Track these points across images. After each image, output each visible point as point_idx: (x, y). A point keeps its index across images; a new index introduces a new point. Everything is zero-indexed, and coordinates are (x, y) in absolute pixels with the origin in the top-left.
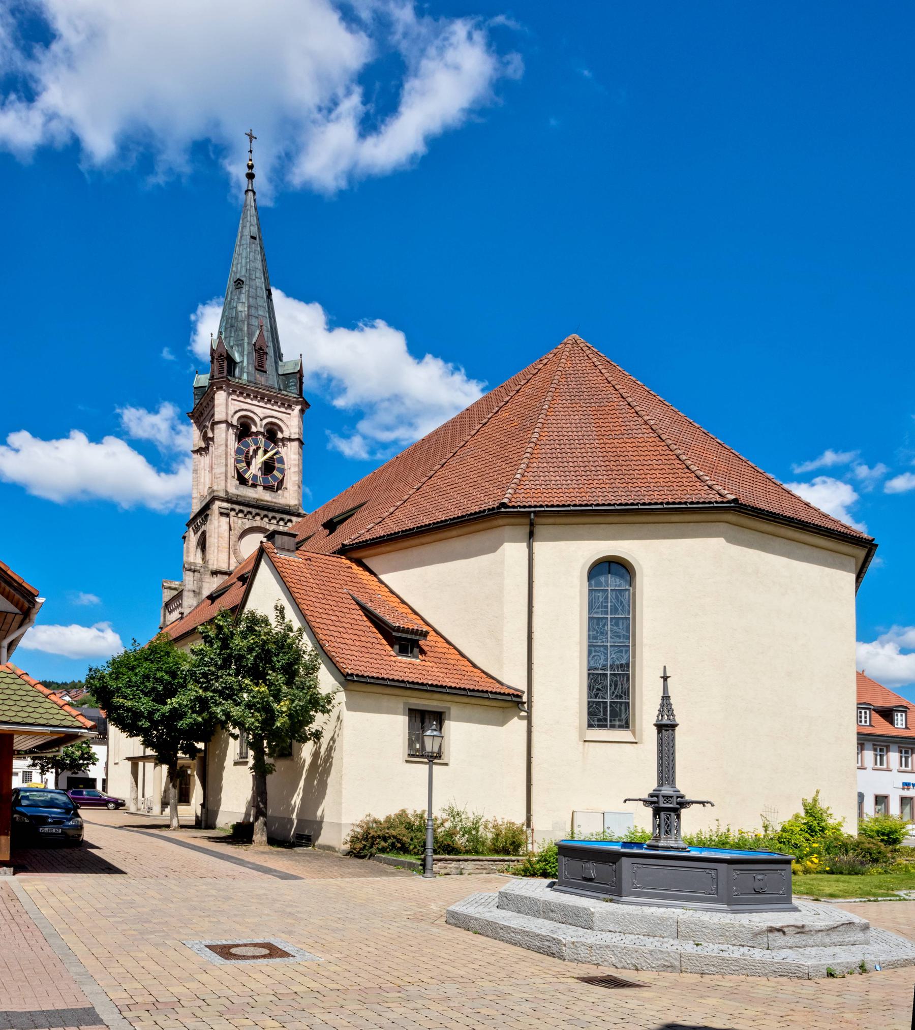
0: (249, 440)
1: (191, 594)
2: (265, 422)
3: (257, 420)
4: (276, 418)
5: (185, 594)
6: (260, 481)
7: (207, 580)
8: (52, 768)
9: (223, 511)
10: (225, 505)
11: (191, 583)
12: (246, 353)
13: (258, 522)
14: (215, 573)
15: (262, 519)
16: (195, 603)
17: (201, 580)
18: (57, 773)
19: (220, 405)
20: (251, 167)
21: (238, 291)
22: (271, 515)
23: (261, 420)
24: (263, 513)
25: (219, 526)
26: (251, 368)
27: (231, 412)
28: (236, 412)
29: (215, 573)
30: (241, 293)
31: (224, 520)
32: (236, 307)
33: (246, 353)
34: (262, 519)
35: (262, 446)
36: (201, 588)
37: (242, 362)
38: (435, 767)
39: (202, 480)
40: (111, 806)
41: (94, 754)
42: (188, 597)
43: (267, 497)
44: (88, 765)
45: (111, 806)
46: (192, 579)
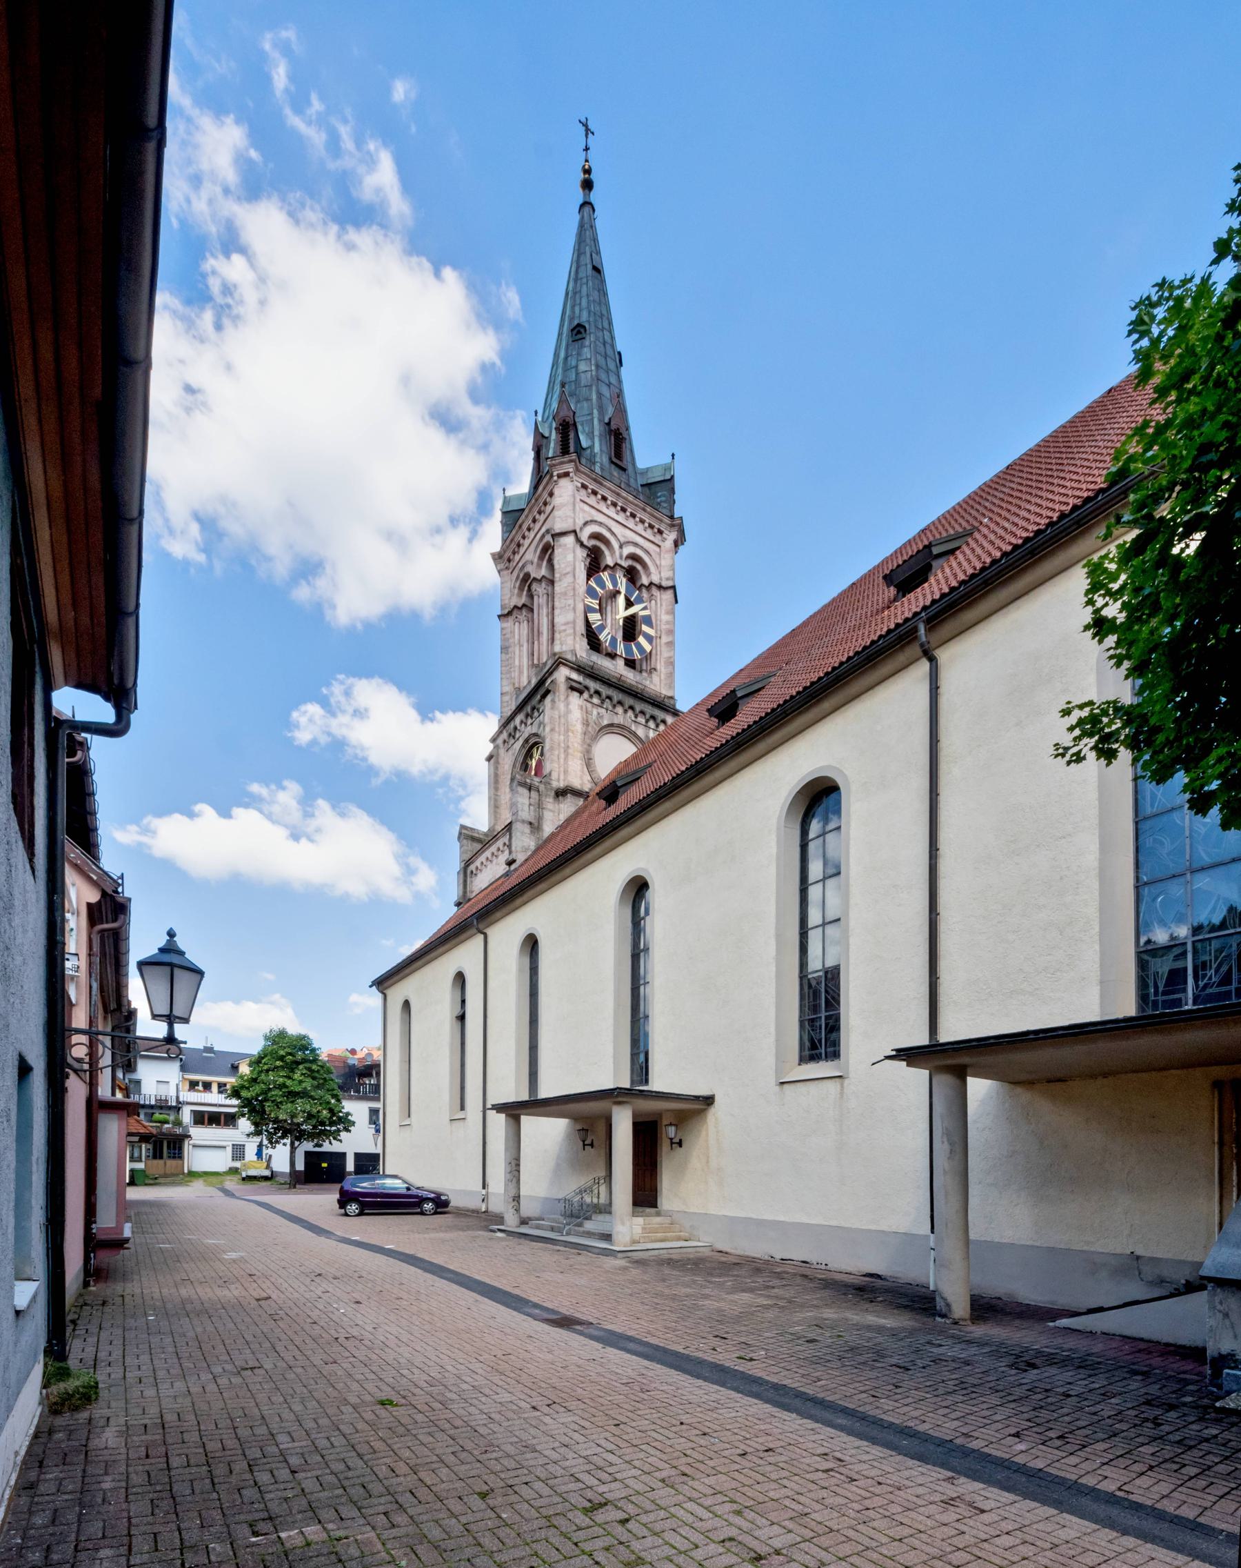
0: (605, 576)
1: (527, 829)
2: (627, 550)
3: (616, 545)
4: (642, 548)
5: (517, 827)
6: (621, 649)
7: (550, 806)
8: (283, 1137)
9: (575, 685)
10: (574, 676)
11: (526, 808)
12: (597, 433)
13: (621, 717)
14: (561, 793)
15: (626, 711)
16: (532, 845)
17: (540, 806)
18: (292, 1144)
19: (563, 505)
20: (587, 171)
21: (577, 345)
22: (639, 706)
23: (621, 547)
24: (629, 701)
25: (568, 712)
26: (605, 460)
27: (580, 522)
28: (586, 524)
29: (561, 793)
30: (583, 346)
31: (575, 700)
32: (577, 367)
33: (597, 433)
34: (626, 711)
35: (623, 591)
36: (540, 819)
37: (592, 447)
38: (387, 1172)
39: (517, 663)
40: (428, 1206)
41: (348, 1114)
42: (523, 833)
43: (630, 676)
44: (339, 1131)
45: (428, 1206)
46: (527, 802)
